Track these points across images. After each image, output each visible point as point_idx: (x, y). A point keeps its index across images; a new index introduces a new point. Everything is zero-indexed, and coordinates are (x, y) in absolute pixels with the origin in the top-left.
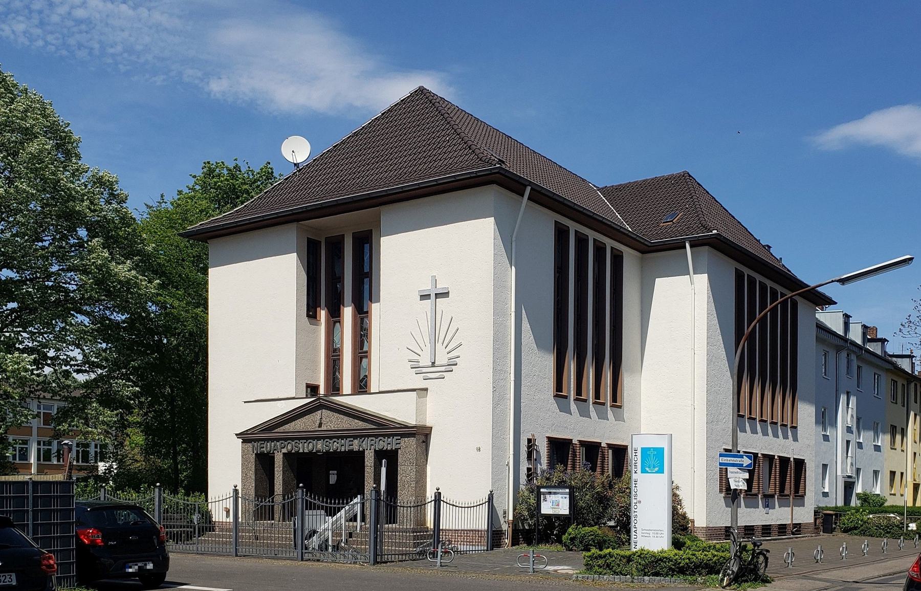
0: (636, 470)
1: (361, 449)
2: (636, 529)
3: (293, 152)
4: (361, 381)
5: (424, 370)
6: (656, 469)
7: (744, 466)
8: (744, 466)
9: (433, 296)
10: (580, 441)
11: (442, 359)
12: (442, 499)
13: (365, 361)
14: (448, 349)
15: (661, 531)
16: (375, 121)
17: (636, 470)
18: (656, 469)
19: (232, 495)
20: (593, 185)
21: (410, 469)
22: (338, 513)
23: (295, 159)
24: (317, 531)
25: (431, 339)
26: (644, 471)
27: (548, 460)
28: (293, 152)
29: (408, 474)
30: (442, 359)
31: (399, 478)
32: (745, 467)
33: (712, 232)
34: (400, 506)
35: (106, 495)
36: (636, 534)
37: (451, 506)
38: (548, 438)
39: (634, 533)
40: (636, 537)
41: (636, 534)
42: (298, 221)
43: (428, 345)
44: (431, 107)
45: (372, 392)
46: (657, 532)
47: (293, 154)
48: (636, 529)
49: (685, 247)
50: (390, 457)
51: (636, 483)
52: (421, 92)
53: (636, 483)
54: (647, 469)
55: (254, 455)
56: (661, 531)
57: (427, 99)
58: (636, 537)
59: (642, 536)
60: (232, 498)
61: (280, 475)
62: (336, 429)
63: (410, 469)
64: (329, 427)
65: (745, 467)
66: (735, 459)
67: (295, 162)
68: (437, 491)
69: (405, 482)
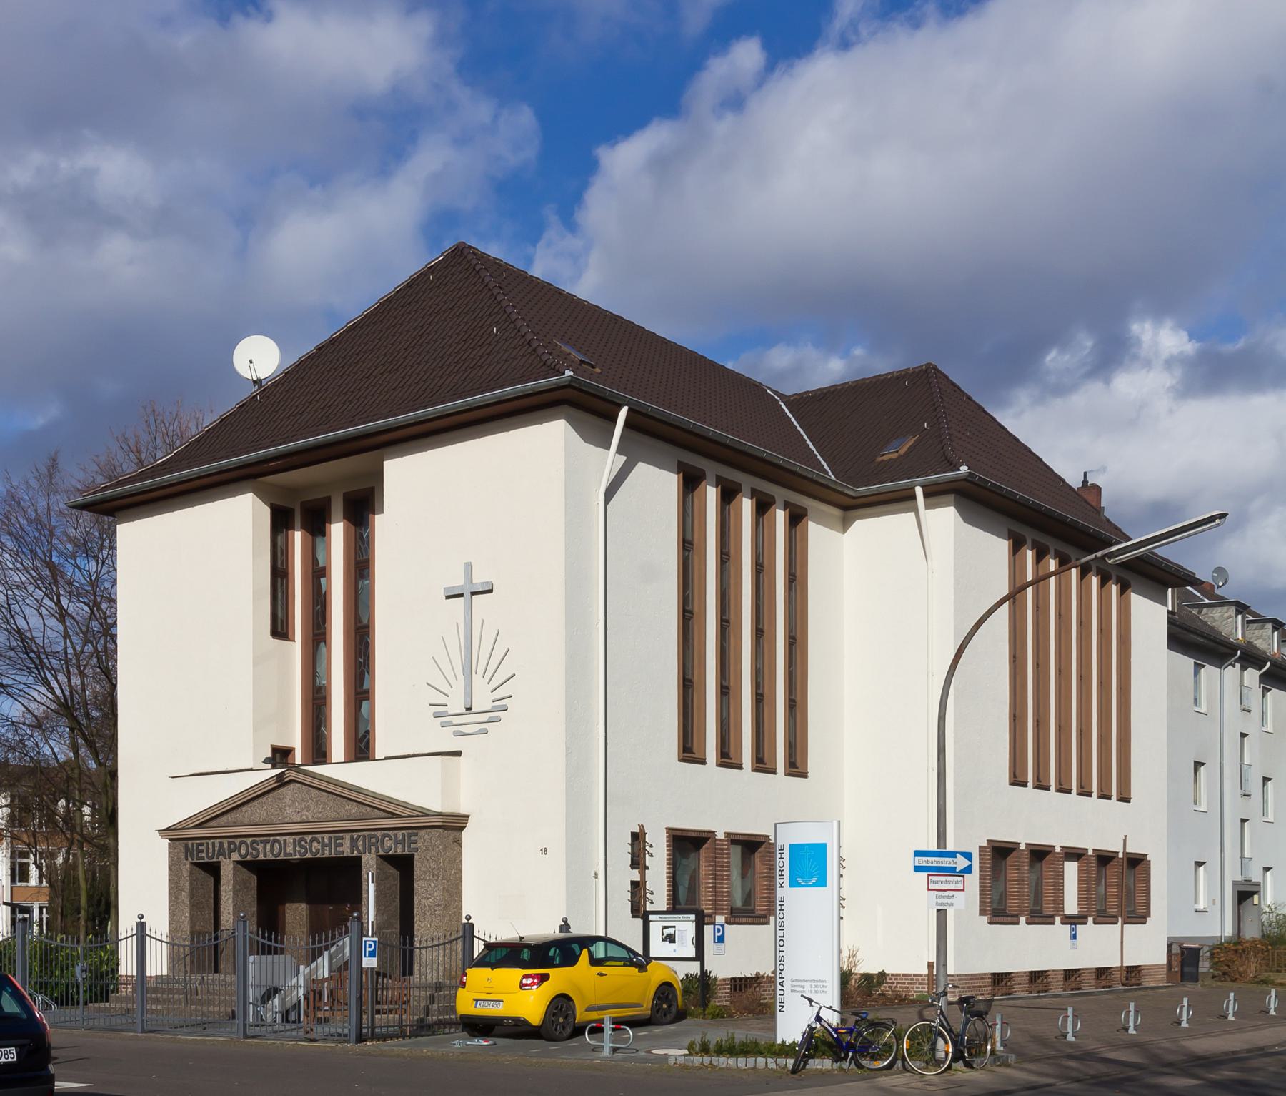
0: (781, 881)
1: (355, 853)
2: (782, 980)
3: (251, 362)
4: (361, 740)
5: (455, 720)
6: (814, 880)
7: (957, 871)
8: (957, 871)
9: (467, 595)
10: (728, 834)
11: (483, 700)
12: (148, 932)
13: (365, 704)
14: (494, 683)
15: (822, 981)
16: (384, 305)
17: (781, 881)
18: (814, 880)
19: (135, 932)
20: (773, 391)
21: (433, 885)
22: (312, 962)
23: (254, 373)
24: (281, 990)
25: (465, 669)
26: (794, 884)
27: (669, 868)
28: (251, 362)
29: (430, 895)
30: (483, 700)
31: (416, 901)
32: (958, 872)
33: (959, 470)
34: (420, 948)
35: (248, 934)
36: (782, 988)
37: (159, 943)
38: (669, 829)
39: (779, 987)
40: (782, 992)
41: (782, 988)
42: (255, 476)
43: (461, 677)
44: (475, 277)
45: (376, 758)
46: (816, 984)
47: (251, 365)
48: (782, 980)
49: (913, 497)
50: (403, 865)
51: (781, 903)
52: (459, 253)
53: (781, 903)
54: (800, 880)
55: (188, 866)
56: (822, 981)
57: (468, 265)
58: (782, 992)
59: (792, 991)
60: (135, 937)
61: (229, 898)
62: (316, 820)
63: (433, 885)
64: (304, 817)
65: (958, 872)
66: (943, 859)
67: (255, 378)
68: (139, 920)
69: (425, 906)
